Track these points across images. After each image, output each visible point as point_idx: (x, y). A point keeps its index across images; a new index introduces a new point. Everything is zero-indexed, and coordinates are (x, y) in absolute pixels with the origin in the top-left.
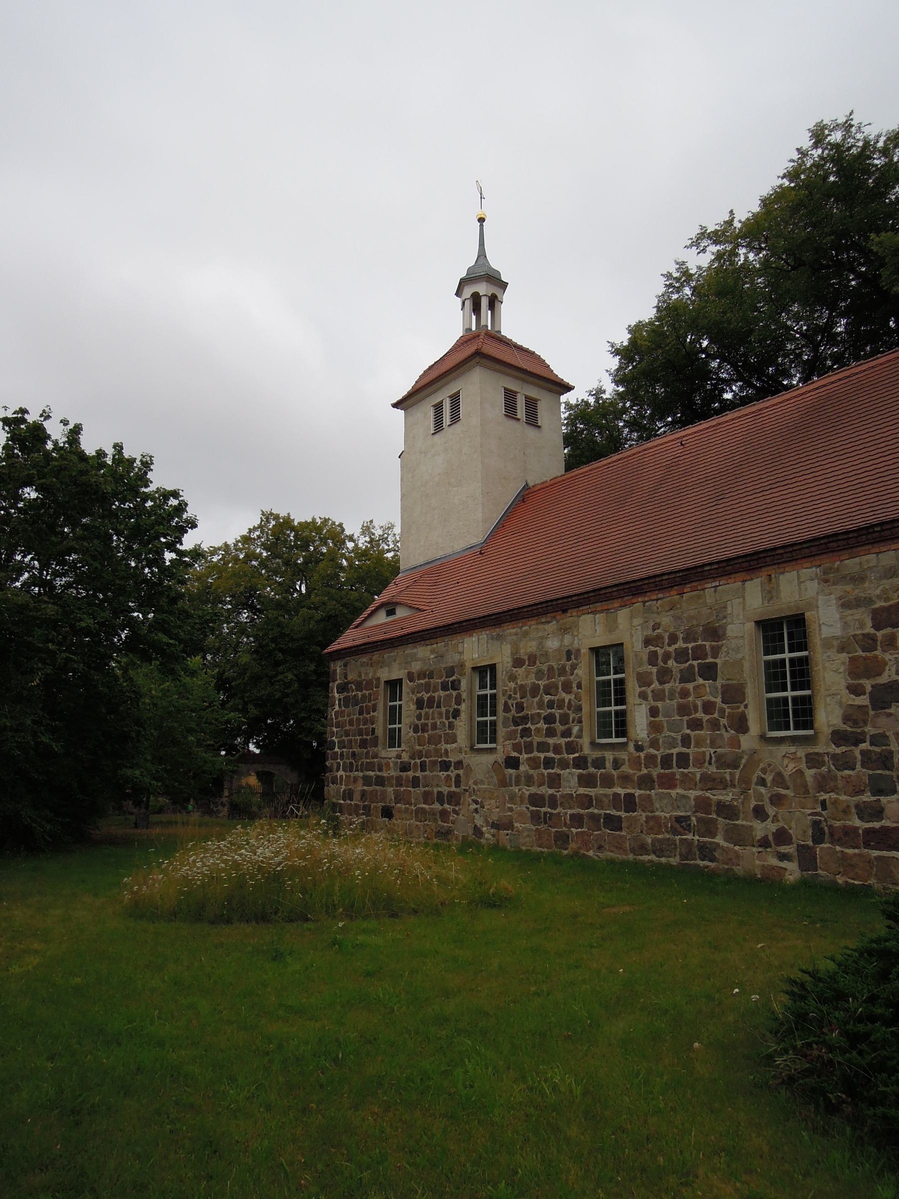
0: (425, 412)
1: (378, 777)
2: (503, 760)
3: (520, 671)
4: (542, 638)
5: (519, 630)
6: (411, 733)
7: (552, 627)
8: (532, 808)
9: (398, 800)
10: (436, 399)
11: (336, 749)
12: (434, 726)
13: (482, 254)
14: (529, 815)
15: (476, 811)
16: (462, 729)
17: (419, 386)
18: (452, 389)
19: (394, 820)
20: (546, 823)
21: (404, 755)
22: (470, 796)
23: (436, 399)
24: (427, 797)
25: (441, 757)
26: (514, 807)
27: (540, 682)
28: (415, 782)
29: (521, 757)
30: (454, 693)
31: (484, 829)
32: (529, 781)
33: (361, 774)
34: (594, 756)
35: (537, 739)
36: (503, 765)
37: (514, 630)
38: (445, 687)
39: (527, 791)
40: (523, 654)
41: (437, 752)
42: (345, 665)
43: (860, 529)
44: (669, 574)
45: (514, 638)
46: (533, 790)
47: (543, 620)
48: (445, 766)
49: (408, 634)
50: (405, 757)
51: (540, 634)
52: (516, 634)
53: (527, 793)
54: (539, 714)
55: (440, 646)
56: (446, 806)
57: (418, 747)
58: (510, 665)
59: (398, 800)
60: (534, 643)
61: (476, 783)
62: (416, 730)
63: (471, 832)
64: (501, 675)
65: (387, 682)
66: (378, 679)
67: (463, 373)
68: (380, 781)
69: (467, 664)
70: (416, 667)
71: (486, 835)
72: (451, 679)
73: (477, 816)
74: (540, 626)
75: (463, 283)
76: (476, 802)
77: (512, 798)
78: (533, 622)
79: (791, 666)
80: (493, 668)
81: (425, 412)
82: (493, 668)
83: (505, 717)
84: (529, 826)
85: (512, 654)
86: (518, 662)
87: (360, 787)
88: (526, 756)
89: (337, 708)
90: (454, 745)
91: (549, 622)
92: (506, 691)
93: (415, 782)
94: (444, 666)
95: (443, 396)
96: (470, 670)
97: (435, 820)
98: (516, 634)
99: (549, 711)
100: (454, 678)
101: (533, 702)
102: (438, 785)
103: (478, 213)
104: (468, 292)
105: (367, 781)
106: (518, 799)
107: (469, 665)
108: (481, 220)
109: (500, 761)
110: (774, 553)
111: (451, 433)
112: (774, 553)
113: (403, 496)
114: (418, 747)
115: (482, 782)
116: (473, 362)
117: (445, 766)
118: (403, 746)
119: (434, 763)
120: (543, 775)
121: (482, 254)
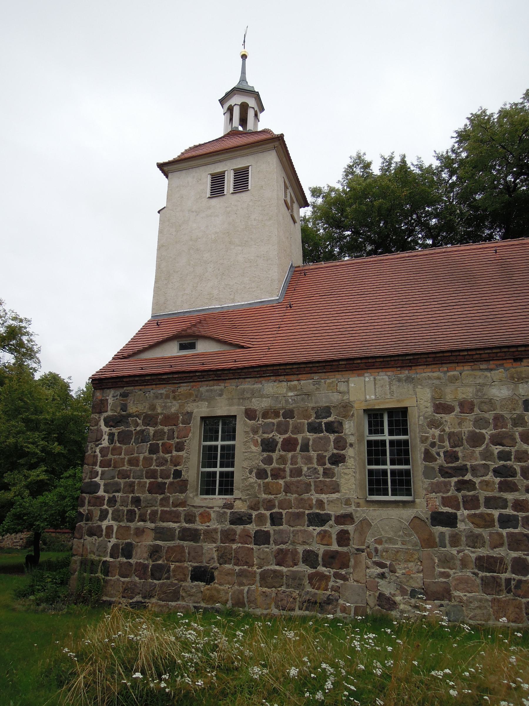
0: (200, 179)
2: (429, 516)
3: (448, 418)
4: (484, 385)
5: (442, 375)
6: (253, 479)
7: (499, 373)
8: (481, 574)
9: (224, 558)
10: (218, 169)
11: (101, 493)
12: (298, 472)
13: (243, 79)
14: (479, 581)
15: (382, 576)
16: (351, 476)
17: (186, 156)
18: (240, 163)
19: (215, 585)
20: (509, 591)
21: (238, 504)
22: (369, 556)
23: (218, 169)
24: (281, 558)
26: (451, 572)
27: (484, 431)
28: (262, 538)
29: (459, 513)
30: (332, 437)
31: (398, 599)
32: (475, 541)
33: (153, 525)
35: (483, 494)
36: (429, 522)
37: (436, 374)
38: (314, 428)
39: (473, 554)
40: (449, 398)
41: (301, 502)
42: (125, 395)
43: (325, 361)
45: (437, 382)
46: (483, 552)
47: (482, 367)
48: (319, 520)
49: (118, 377)
50: (240, 507)
51: (481, 381)
52: (439, 378)
53: (474, 556)
54: (486, 466)
55: (306, 383)
56: (321, 569)
57: (264, 496)
58: (430, 410)
59: (224, 558)
60: (470, 390)
61: (379, 541)
62: (261, 474)
63: (372, 602)
64: (415, 420)
65: (203, 419)
66: (190, 414)
67: (257, 152)
69: (355, 405)
70: (259, 404)
71: (402, 607)
72: (325, 420)
73: (381, 582)
74: (478, 373)
76: (381, 565)
77: (446, 561)
78: (466, 368)
80: (404, 411)
81: (200, 179)
82: (404, 411)
83: (426, 467)
84: (479, 595)
85: (433, 398)
86: (442, 408)
87: (148, 541)
88: (466, 512)
89: (105, 443)
90: (335, 496)
91: (491, 370)
92: (427, 438)
93: (262, 538)
94: (311, 405)
95: (228, 168)
96: (199, 419)
97: (300, 586)
98: (439, 378)
99: (502, 463)
100: (330, 419)
101: (474, 452)
102: (304, 543)
106: (458, 563)
107: (359, 407)
108: (244, 57)
109: (423, 516)
110: (404, 358)
111: (230, 199)
112: (404, 358)
113: (160, 247)
114: (264, 496)
115: (390, 540)
116: (271, 145)
117: (319, 520)
118: (237, 494)
119: (299, 516)
120: (500, 535)
121: (243, 79)
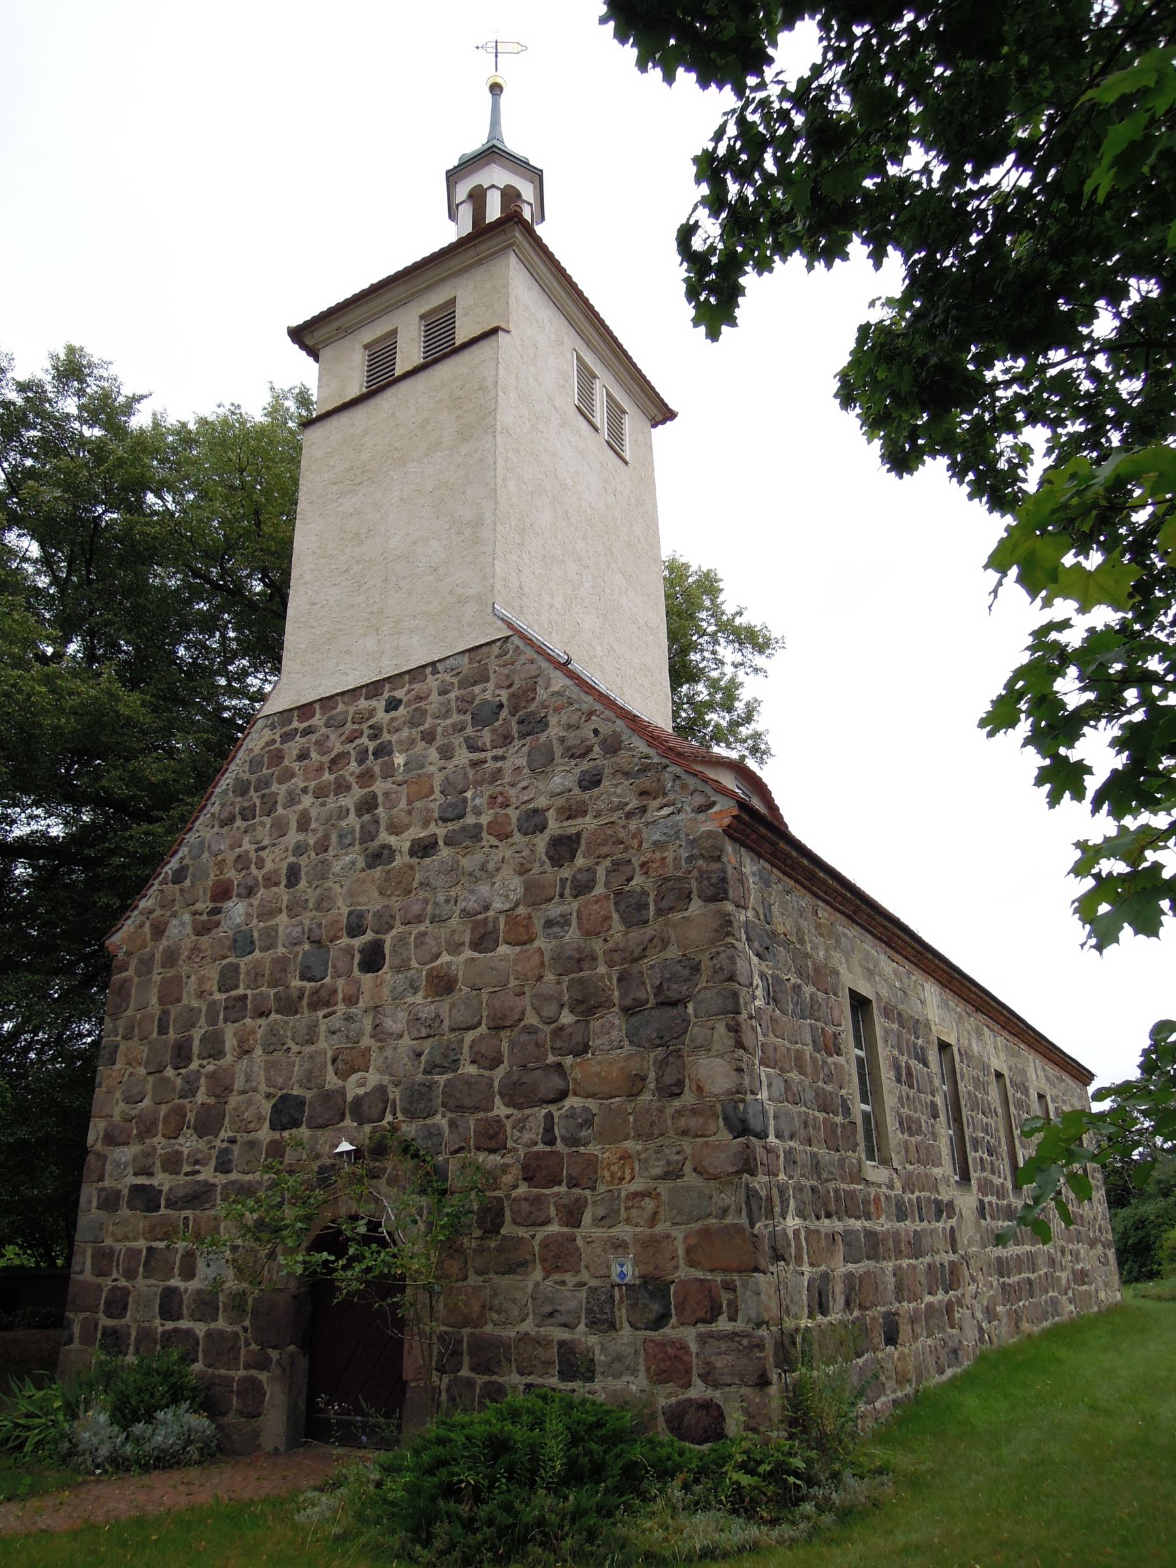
75: (454, 177)
108: (496, 89)
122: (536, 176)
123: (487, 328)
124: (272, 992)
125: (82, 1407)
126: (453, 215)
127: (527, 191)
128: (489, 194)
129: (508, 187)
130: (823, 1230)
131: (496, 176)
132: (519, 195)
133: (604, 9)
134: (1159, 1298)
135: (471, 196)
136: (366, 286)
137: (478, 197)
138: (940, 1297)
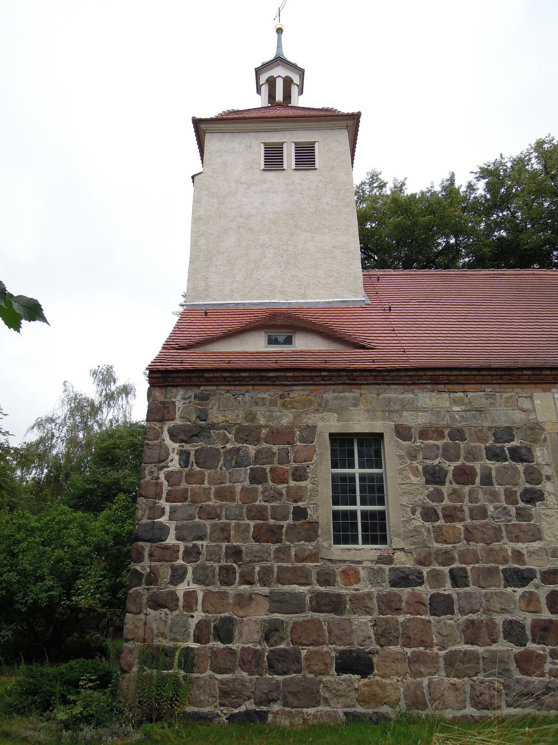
1: (318, 596)
24: (472, 632)
25: (506, 561)
28: (441, 605)
34: (432, 593)
44: (421, 384)
50: (404, 561)
56: (531, 646)
68: (335, 604)
70: (416, 420)
75: (258, 71)
79: (362, 519)
102: (503, 610)
103: (276, 24)
104: (263, 78)
105: (279, 602)
108: (279, 31)
116: (344, 123)
119: (491, 572)
122: (301, 72)
123: (298, 171)
124: (252, 523)
125: (521, 741)
126: (259, 91)
127: (296, 79)
128: (277, 80)
129: (287, 77)
130: (208, 541)
131: (279, 72)
132: (292, 81)
133: (433, 140)
134: (108, 414)
135: (267, 81)
136: (204, 118)
137: (271, 82)
138: (481, 662)
